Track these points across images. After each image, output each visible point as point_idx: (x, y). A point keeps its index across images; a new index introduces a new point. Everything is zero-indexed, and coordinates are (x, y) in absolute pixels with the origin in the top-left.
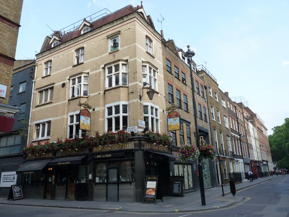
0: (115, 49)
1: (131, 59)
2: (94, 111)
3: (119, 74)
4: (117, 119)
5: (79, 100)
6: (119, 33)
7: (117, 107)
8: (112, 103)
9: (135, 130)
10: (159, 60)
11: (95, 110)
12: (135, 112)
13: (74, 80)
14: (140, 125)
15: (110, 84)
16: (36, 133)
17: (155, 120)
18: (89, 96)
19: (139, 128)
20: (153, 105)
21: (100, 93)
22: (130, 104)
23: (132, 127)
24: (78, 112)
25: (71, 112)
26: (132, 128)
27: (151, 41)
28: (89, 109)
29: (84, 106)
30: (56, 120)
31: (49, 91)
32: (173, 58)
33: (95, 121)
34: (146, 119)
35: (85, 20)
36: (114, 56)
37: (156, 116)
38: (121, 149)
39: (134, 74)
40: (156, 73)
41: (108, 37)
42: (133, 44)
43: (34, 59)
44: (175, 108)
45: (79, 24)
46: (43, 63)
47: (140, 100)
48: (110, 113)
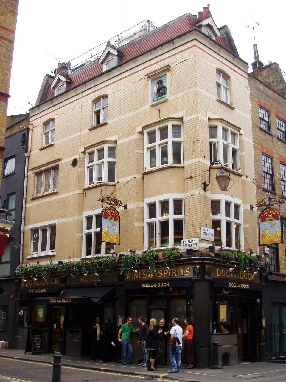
0: (160, 98)
1: (189, 117)
2: (125, 210)
3: (168, 143)
4: (165, 225)
5: (100, 190)
6: (168, 68)
7: (164, 205)
8: (155, 195)
9: (194, 245)
10: (244, 111)
11: (128, 207)
12: (194, 213)
13: (91, 154)
14: (204, 237)
15: (152, 163)
16: (32, 244)
17: (234, 226)
18: (118, 182)
19: (202, 241)
20: (230, 199)
21: (135, 178)
22: (187, 198)
23: (190, 239)
24: (99, 211)
25: (88, 210)
26: (190, 241)
27: (226, 77)
28: (116, 207)
29: (109, 202)
30: (64, 223)
31: (52, 173)
32: (274, 103)
33: (128, 226)
34: (216, 224)
35: (109, 44)
36: (159, 110)
37: (237, 217)
38: (171, 278)
39: (193, 144)
40: (238, 138)
41: (149, 77)
42: (192, 89)
43: (27, 112)
44: (272, 201)
45: (99, 51)
46: (41, 124)
47: (204, 191)
48: (152, 214)
